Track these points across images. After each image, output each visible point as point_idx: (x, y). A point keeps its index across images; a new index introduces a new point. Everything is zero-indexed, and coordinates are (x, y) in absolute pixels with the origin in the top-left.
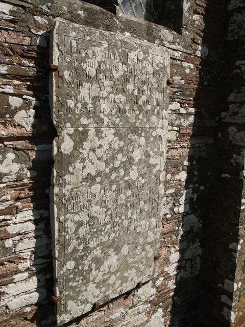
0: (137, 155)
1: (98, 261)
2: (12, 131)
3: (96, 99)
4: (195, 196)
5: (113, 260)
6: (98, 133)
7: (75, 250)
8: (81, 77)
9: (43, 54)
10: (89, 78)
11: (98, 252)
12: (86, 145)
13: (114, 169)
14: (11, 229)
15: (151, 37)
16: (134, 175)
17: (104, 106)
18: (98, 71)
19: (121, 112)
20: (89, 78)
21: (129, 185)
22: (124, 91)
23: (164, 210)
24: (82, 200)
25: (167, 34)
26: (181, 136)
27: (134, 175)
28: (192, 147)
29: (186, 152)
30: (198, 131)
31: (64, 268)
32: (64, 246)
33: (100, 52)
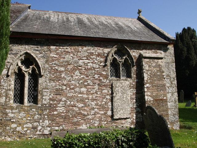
0: (125, 96)
1: (120, 111)
2: (109, 93)
3: (118, 89)
4: (138, 105)
5: (122, 111)
6: (119, 93)
7: (116, 108)
8: (116, 87)
9: (112, 85)
10: (117, 87)
11: (119, 109)
12: (117, 95)
13: (121, 98)
14: (109, 104)
15: (126, 80)
16: (124, 99)
17: (119, 90)
18: (118, 86)
19: (122, 91)
20: (117, 87)
21: (124, 101)
22: (122, 88)
23: (131, 106)
24: (117, 102)
25: (129, 79)
26: (134, 94)
27: (124, 99)
28: (136, 96)
29: (135, 97)
30: (137, 93)
31: (115, 110)
32: (115, 107)
33: (118, 84)
